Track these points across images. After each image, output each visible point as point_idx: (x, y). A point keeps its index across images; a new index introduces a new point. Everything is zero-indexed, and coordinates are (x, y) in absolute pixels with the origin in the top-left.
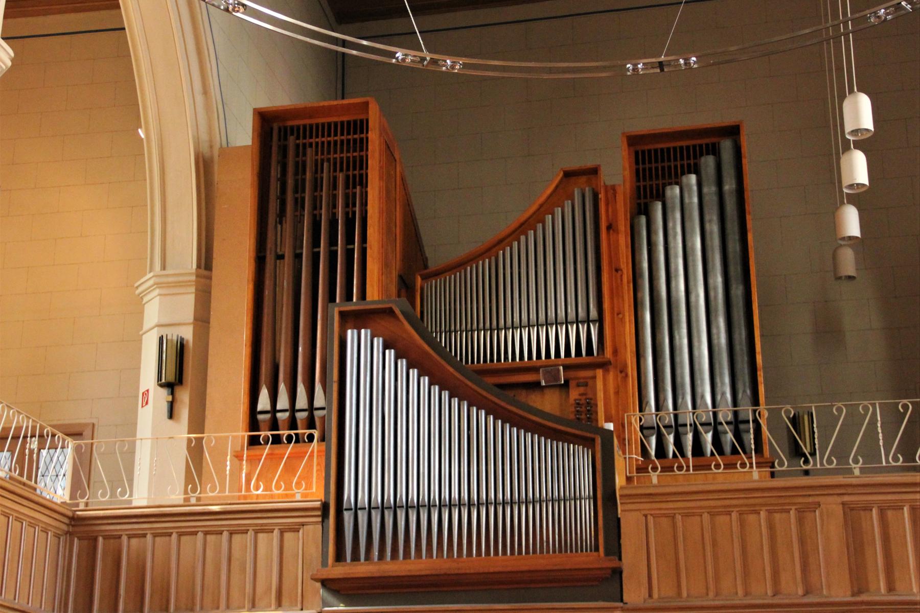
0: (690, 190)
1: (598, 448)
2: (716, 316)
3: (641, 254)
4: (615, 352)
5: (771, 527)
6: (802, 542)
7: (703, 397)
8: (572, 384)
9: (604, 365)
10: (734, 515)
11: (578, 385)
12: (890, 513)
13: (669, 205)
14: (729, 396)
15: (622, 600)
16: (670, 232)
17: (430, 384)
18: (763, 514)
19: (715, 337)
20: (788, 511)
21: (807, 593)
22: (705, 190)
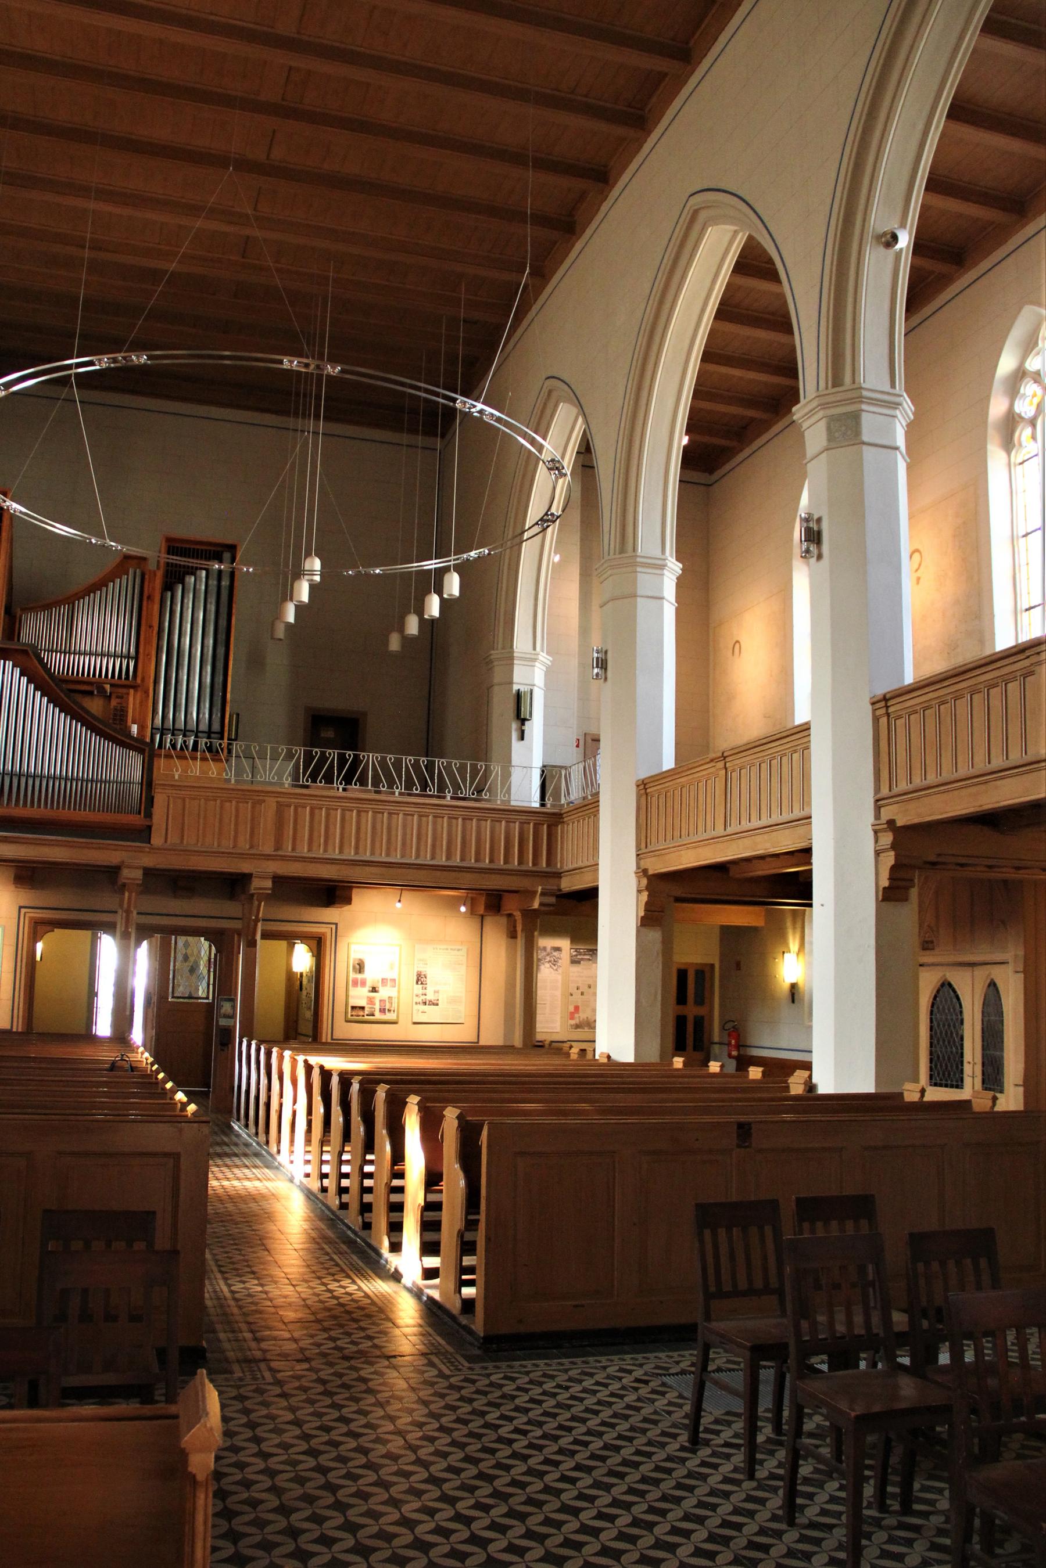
0: (201, 581)
1: (147, 754)
2: (207, 665)
3: (165, 617)
4: (143, 679)
5: (237, 810)
6: (253, 819)
7: (192, 714)
8: (113, 696)
9: (135, 687)
10: (218, 802)
11: (118, 697)
12: (300, 809)
13: (186, 586)
14: (207, 716)
15: (149, 843)
16: (185, 605)
17: (48, 702)
18: (234, 803)
19: (203, 678)
20: (247, 803)
21: (251, 847)
22: (210, 582)
